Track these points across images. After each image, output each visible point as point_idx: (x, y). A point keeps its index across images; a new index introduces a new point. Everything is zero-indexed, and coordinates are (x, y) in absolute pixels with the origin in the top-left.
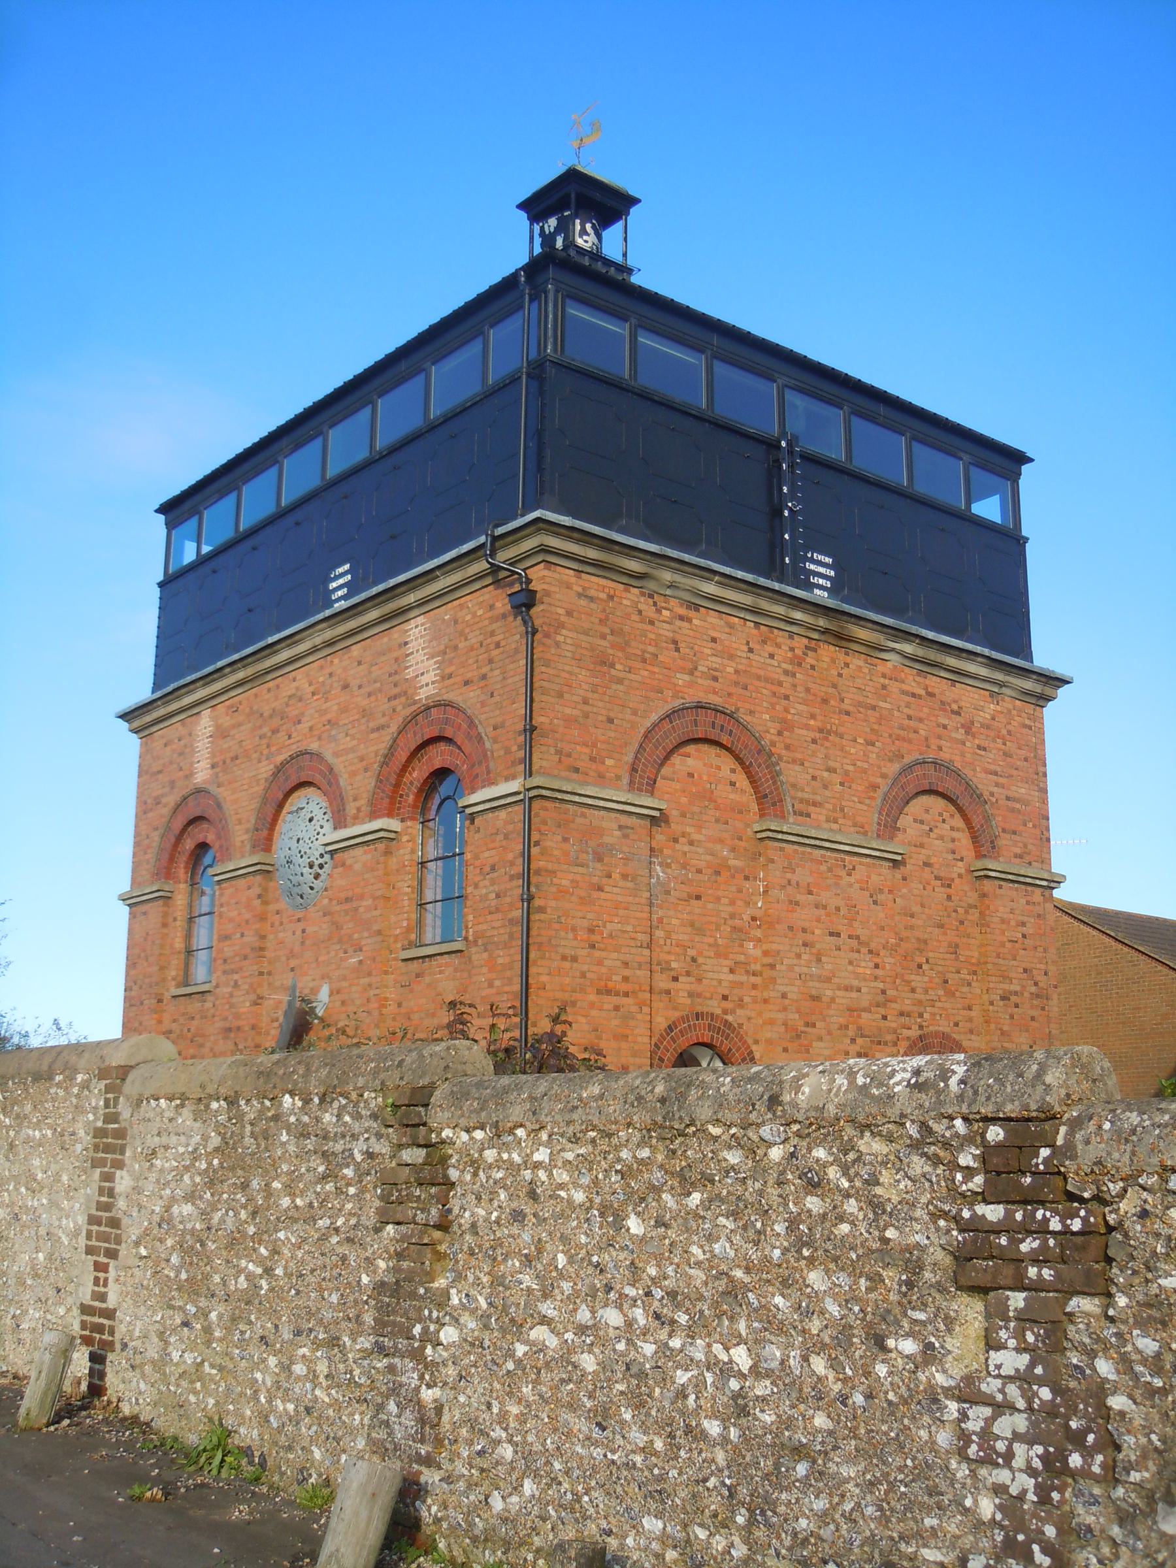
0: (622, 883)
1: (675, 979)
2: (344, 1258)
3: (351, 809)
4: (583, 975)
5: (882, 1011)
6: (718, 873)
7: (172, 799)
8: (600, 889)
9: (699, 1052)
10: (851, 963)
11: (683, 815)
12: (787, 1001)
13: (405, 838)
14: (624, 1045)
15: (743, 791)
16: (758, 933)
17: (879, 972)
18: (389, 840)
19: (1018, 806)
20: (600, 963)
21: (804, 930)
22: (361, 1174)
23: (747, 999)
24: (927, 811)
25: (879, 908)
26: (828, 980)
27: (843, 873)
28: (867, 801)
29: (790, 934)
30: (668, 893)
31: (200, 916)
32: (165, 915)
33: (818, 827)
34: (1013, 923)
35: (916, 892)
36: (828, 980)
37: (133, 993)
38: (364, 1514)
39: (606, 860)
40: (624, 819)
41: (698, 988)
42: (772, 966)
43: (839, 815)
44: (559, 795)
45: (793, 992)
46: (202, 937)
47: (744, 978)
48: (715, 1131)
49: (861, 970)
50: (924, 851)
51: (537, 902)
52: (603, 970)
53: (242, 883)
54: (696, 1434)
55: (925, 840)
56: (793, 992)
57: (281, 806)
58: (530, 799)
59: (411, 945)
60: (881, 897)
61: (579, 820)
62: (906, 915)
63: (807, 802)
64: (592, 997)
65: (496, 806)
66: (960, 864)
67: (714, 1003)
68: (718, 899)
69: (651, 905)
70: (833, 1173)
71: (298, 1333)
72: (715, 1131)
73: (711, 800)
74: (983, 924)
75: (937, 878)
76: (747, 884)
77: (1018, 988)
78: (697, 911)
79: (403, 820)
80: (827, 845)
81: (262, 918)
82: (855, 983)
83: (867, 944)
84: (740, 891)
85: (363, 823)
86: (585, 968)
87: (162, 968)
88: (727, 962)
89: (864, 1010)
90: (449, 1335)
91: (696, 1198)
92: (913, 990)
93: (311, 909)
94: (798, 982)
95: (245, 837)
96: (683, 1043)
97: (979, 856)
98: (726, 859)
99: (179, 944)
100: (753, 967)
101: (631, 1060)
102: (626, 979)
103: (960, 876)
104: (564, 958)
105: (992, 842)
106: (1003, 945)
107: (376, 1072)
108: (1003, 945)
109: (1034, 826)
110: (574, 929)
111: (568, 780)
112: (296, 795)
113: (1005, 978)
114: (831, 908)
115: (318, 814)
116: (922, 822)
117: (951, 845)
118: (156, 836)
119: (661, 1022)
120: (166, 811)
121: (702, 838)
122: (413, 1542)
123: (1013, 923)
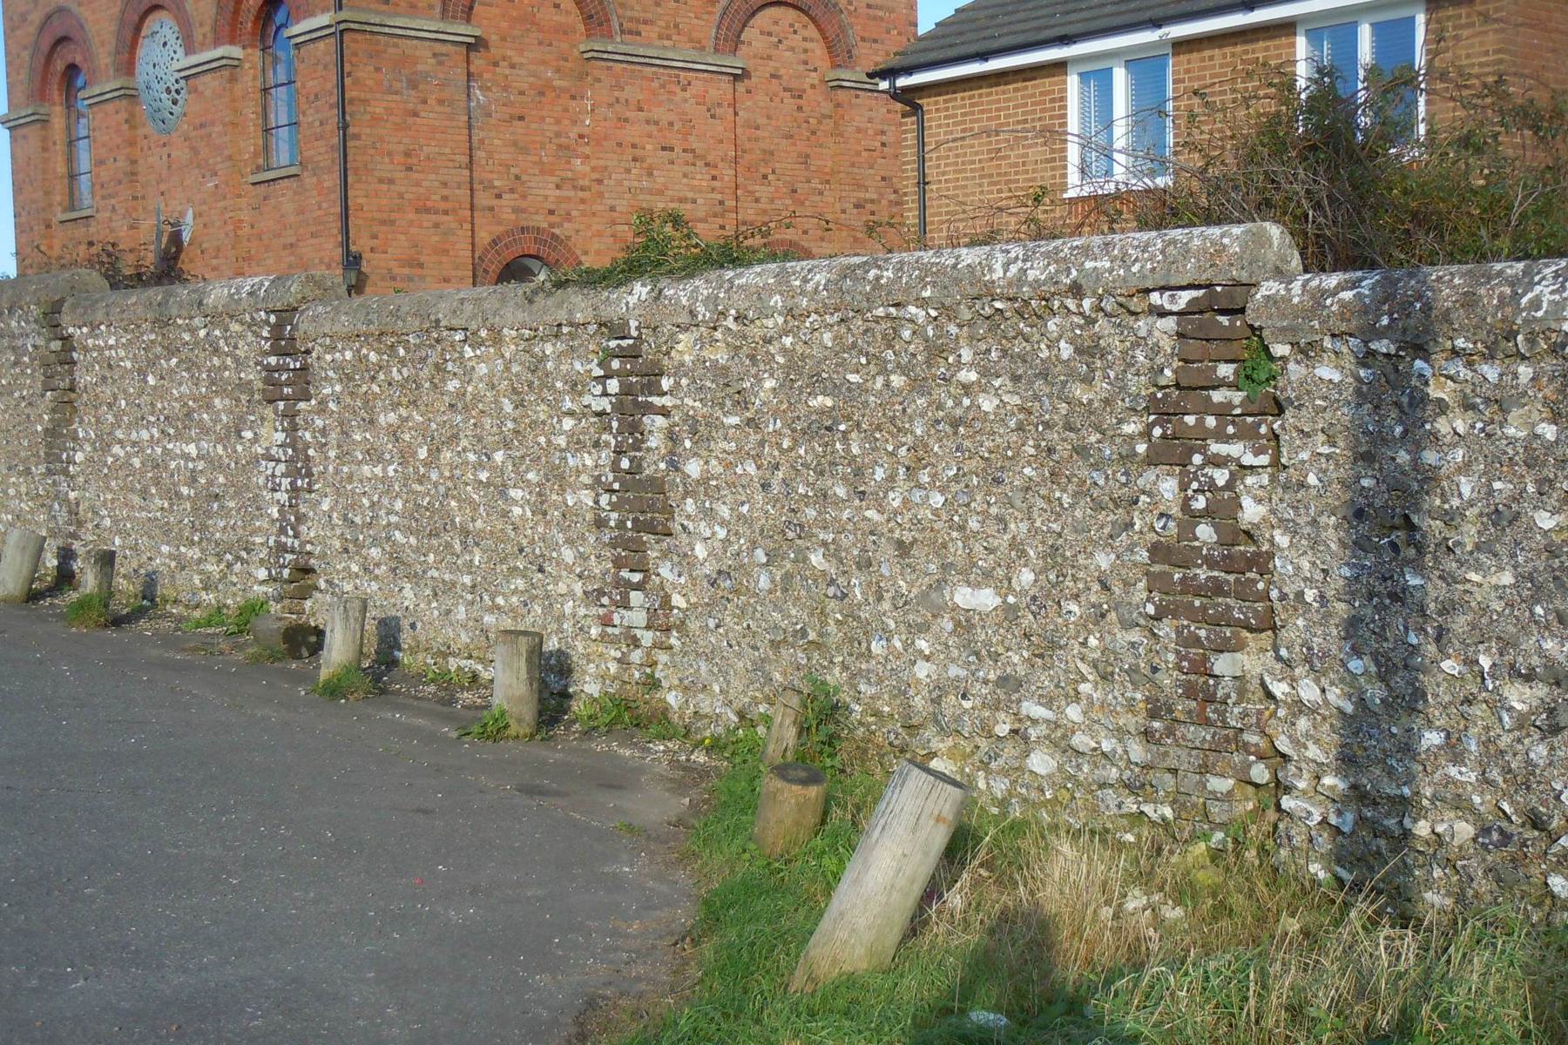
0: (438, 108)
1: (499, 196)
2: (28, 416)
3: (198, 34)
4: (401, 196)
5: (720, 221)
6: (542, 94)
7: (36, 17)
8: (416, 114)
9: (533, 264)
10: (685, 176)
11: (503, 39)
12: (615, 215)
13: (247, 66)
14: (444, 259)
15: (568, 13)
16: (587, 150)
17: (717, 184)
18: (231, 68)
19: (880, 13)
20: (418, 184)
21: (634, 146)
22: (32, 360)
23: (574, 213)
24: (776, 23)
25: (717, 122)
26: (661, 192)
27: (677, 89)
28: (705, 17)
29: (619, 150)
30: (490, 115)
31: (277, 86)
32: (44, 139)
33: (649, 45)
34: (870, 132)
35: (761, 104)
36: (661, 192)
37: (23, 219)
38: (18, 558)
39: (421, 87)
40: (438, 47)
41: (524, 204)
42: (600, 182)
43: (673, 31)
44: (368, 28)
45: (622, 205)
46: (84, 162)
47: (571, 193)
48: (180, 322)
49: (696, 183)
50: (771, 63)
51: (351, 130)
52: (421, 190)
53: (110, 107)
54: (178, 495)
55: (774, 52)
56: (622, 205)
57: (138, 29)
58: (341, 33)
59: (259, 169)
60: (719, 111)
61: (391, 50)
62: (749, 127)
63: (638, 21)
64: (412, 216)
65: (315, 37)
66: (813, 74)
67: (539, 218)
68: (543, 119)
69: (470, 128)
70: (222, 342)
71: (9, 469)
72: (180, 322)
73: (533, 23)
74: (837, 133)
75: (785, 90)
76: (573, 103)
77: (875, 196)
78: (521, 131)
79: (244, 48)
80: (658, 62)
81: (132, 143)
82: (690, 195)
83: (703, 157)
84: (566, 110)
85: (209, 49)
86: (403, 189)
87: (47, 193)
88: (555, 179)
89: (700, 220)
90: (79, 457)
91: (174, 360)
92: (757, 200)
93: (174, 134)
94: (627, 196)
95: (108, 60)
96: (508, 256)
97: (835, 66)
98: (550, 80)
99: (61, 169)
100: (581, 182)
101: (454, 273)
102: (445, 198)
103: (813, 86)
104: (381, 181)
105: (849, 52)
106: (858, 153)
107: (36, 291)
108: (858, 153)
109: (899, 34)
110: (390, 154)
111: (378, 13)
112: (151, 17)
113: (859, 186)
114: (664, 123)
115: (171, 38)
116: (770, 34)
117: (803, 56)
118: (26, 55)
119: (484, 237)
120: (32, 29)
121: (524, 61)
122: (70, 584)
123: (870, 132)
